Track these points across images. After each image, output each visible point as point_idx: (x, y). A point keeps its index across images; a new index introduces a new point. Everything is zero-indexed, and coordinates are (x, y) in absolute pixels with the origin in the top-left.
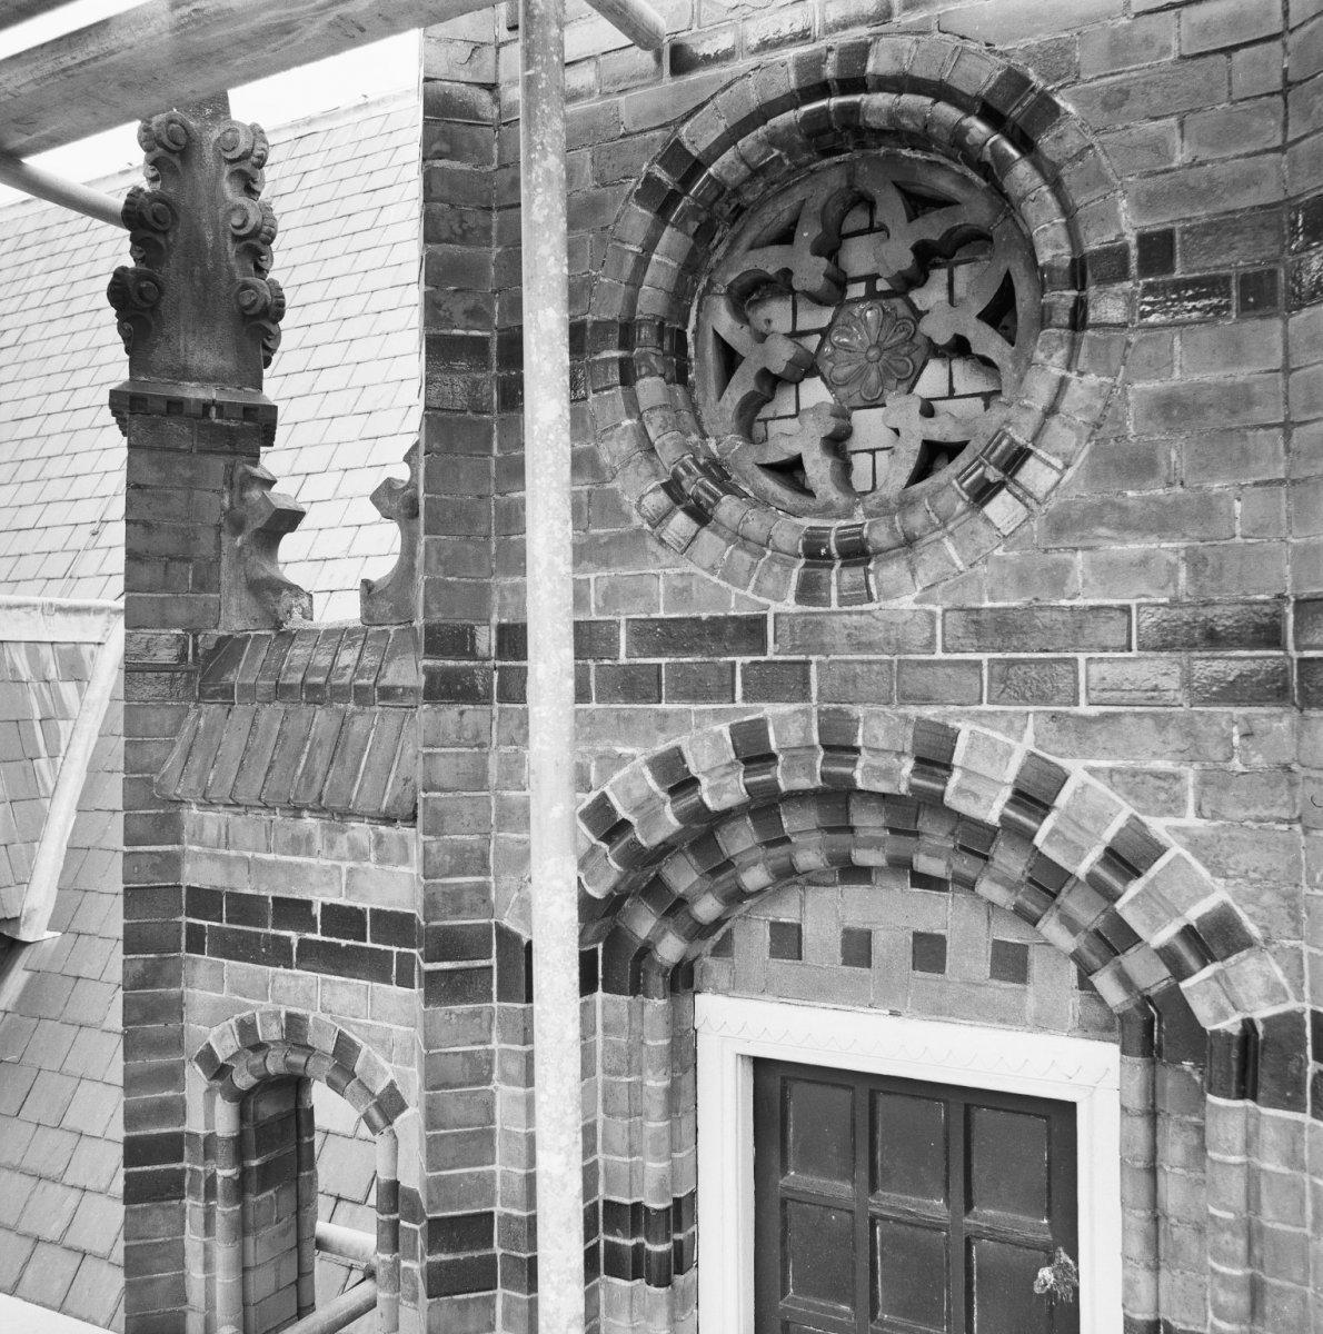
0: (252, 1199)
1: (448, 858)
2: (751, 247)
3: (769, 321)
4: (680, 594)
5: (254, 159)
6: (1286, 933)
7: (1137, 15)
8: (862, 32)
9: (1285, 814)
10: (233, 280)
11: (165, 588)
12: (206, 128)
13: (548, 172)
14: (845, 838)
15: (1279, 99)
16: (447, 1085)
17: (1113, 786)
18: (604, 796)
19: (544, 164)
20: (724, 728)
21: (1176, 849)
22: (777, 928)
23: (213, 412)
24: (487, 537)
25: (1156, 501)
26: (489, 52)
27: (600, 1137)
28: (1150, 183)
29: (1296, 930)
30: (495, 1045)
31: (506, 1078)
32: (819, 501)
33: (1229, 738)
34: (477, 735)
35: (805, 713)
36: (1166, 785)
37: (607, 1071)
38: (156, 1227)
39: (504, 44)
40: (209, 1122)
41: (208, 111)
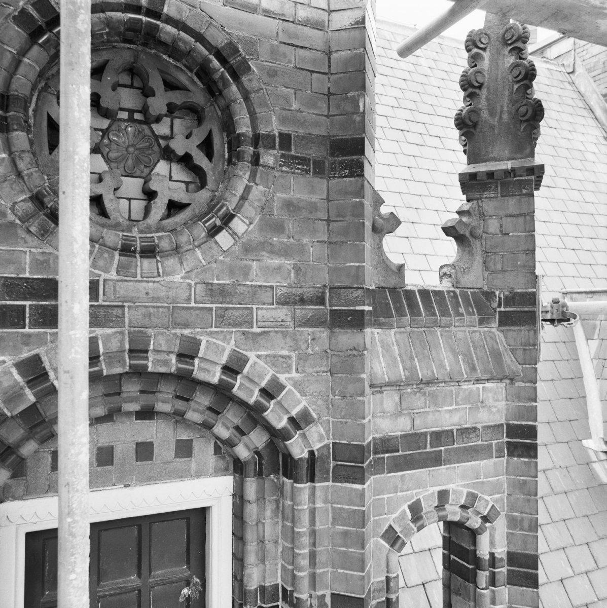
6: (326, 414)
21: (289, 387)
35: (122, 333)
36: (286, 360)
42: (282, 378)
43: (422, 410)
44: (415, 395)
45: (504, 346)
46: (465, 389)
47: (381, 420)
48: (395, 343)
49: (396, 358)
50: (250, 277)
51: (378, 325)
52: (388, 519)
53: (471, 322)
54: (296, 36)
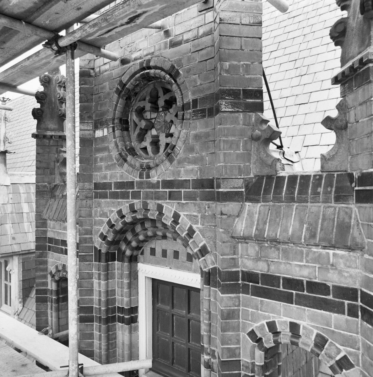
0: (60, 304)
1: (84, 231)
2: (139, 101)
3: (146, 116)
4: (121, 176)
5: (62, 83)
6: (214, 250)
7: (192, 53)
8: (149, 57)
9: (214, 225)
10: (58, 109)
11: (43, 175)
12: (54, 76)
13: (69, 97)
14: (156, 229)
15: (214, 71)
16: (84, 279)
17: (187, 218)
18: (110, 219)
19: (69, 95)
20: (128, 205)
21: (197, 232)
22: (151, 248)
23: (53, 137)
24: (92, 164)
25: (194, 157)
26: (92, 62)
27: (116, 292)
28: (194, 89)
29: (216, 250)
30: (94, 271)
31: (95, 278)
32: (149, 156)
33: (205, 208)
34: (90, 206)
35: (140, 202)
36: (195, 218)
37: (118, 278)
38: (42, 308)
39: (95, 59)
40: (51, 288)
41: (54, 73)
42: (194, 227)
43: (276, 260)
44: (271, 248)
45: (358, 221)
46: (315, 252)
47: (246, 260)
48: (258, 213)
49: (254, 222)
50: (181, 176)
51: (249, 200)
52: (252, 325)
53: (326, 199)
54: (199, 45)
